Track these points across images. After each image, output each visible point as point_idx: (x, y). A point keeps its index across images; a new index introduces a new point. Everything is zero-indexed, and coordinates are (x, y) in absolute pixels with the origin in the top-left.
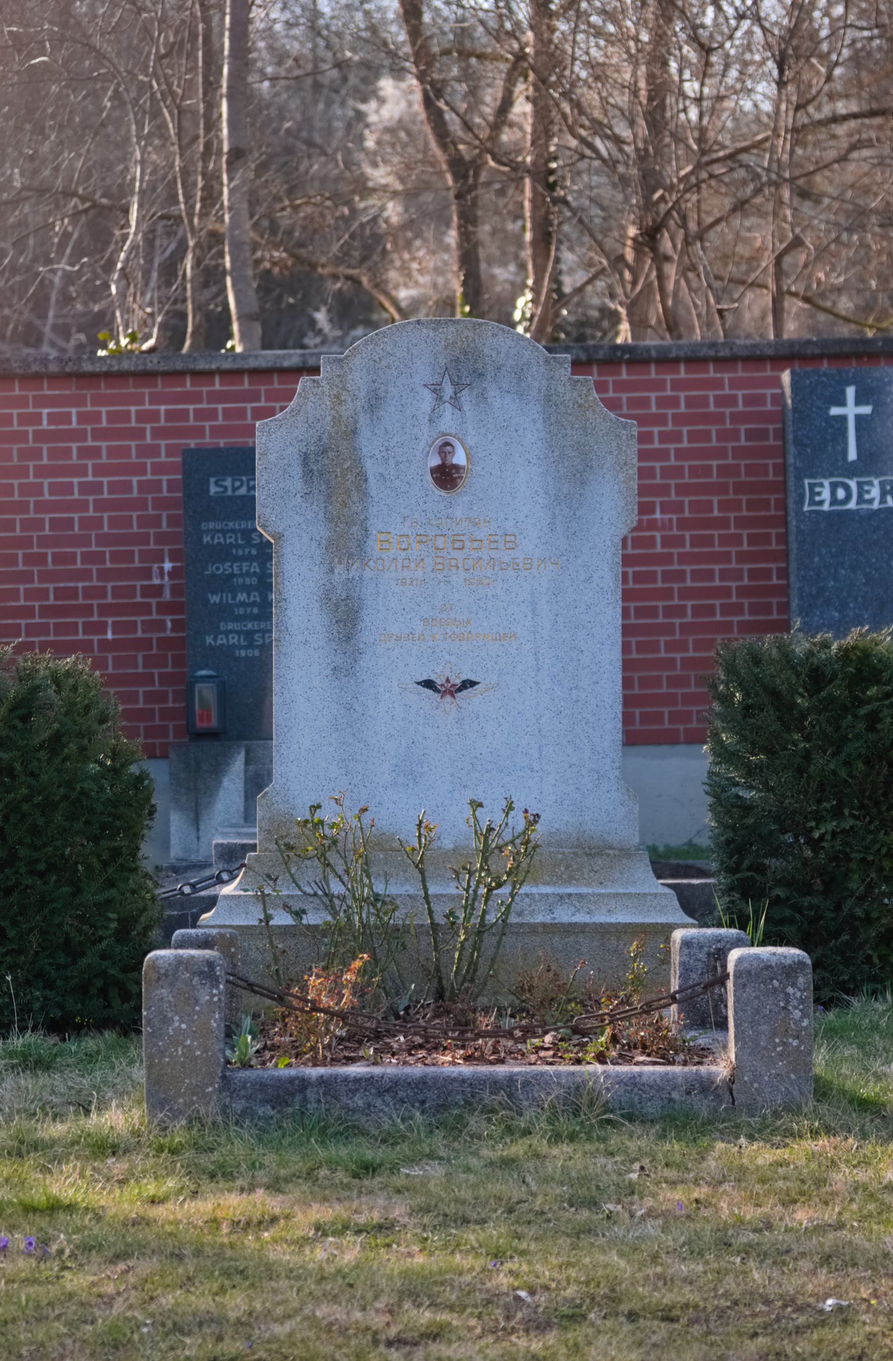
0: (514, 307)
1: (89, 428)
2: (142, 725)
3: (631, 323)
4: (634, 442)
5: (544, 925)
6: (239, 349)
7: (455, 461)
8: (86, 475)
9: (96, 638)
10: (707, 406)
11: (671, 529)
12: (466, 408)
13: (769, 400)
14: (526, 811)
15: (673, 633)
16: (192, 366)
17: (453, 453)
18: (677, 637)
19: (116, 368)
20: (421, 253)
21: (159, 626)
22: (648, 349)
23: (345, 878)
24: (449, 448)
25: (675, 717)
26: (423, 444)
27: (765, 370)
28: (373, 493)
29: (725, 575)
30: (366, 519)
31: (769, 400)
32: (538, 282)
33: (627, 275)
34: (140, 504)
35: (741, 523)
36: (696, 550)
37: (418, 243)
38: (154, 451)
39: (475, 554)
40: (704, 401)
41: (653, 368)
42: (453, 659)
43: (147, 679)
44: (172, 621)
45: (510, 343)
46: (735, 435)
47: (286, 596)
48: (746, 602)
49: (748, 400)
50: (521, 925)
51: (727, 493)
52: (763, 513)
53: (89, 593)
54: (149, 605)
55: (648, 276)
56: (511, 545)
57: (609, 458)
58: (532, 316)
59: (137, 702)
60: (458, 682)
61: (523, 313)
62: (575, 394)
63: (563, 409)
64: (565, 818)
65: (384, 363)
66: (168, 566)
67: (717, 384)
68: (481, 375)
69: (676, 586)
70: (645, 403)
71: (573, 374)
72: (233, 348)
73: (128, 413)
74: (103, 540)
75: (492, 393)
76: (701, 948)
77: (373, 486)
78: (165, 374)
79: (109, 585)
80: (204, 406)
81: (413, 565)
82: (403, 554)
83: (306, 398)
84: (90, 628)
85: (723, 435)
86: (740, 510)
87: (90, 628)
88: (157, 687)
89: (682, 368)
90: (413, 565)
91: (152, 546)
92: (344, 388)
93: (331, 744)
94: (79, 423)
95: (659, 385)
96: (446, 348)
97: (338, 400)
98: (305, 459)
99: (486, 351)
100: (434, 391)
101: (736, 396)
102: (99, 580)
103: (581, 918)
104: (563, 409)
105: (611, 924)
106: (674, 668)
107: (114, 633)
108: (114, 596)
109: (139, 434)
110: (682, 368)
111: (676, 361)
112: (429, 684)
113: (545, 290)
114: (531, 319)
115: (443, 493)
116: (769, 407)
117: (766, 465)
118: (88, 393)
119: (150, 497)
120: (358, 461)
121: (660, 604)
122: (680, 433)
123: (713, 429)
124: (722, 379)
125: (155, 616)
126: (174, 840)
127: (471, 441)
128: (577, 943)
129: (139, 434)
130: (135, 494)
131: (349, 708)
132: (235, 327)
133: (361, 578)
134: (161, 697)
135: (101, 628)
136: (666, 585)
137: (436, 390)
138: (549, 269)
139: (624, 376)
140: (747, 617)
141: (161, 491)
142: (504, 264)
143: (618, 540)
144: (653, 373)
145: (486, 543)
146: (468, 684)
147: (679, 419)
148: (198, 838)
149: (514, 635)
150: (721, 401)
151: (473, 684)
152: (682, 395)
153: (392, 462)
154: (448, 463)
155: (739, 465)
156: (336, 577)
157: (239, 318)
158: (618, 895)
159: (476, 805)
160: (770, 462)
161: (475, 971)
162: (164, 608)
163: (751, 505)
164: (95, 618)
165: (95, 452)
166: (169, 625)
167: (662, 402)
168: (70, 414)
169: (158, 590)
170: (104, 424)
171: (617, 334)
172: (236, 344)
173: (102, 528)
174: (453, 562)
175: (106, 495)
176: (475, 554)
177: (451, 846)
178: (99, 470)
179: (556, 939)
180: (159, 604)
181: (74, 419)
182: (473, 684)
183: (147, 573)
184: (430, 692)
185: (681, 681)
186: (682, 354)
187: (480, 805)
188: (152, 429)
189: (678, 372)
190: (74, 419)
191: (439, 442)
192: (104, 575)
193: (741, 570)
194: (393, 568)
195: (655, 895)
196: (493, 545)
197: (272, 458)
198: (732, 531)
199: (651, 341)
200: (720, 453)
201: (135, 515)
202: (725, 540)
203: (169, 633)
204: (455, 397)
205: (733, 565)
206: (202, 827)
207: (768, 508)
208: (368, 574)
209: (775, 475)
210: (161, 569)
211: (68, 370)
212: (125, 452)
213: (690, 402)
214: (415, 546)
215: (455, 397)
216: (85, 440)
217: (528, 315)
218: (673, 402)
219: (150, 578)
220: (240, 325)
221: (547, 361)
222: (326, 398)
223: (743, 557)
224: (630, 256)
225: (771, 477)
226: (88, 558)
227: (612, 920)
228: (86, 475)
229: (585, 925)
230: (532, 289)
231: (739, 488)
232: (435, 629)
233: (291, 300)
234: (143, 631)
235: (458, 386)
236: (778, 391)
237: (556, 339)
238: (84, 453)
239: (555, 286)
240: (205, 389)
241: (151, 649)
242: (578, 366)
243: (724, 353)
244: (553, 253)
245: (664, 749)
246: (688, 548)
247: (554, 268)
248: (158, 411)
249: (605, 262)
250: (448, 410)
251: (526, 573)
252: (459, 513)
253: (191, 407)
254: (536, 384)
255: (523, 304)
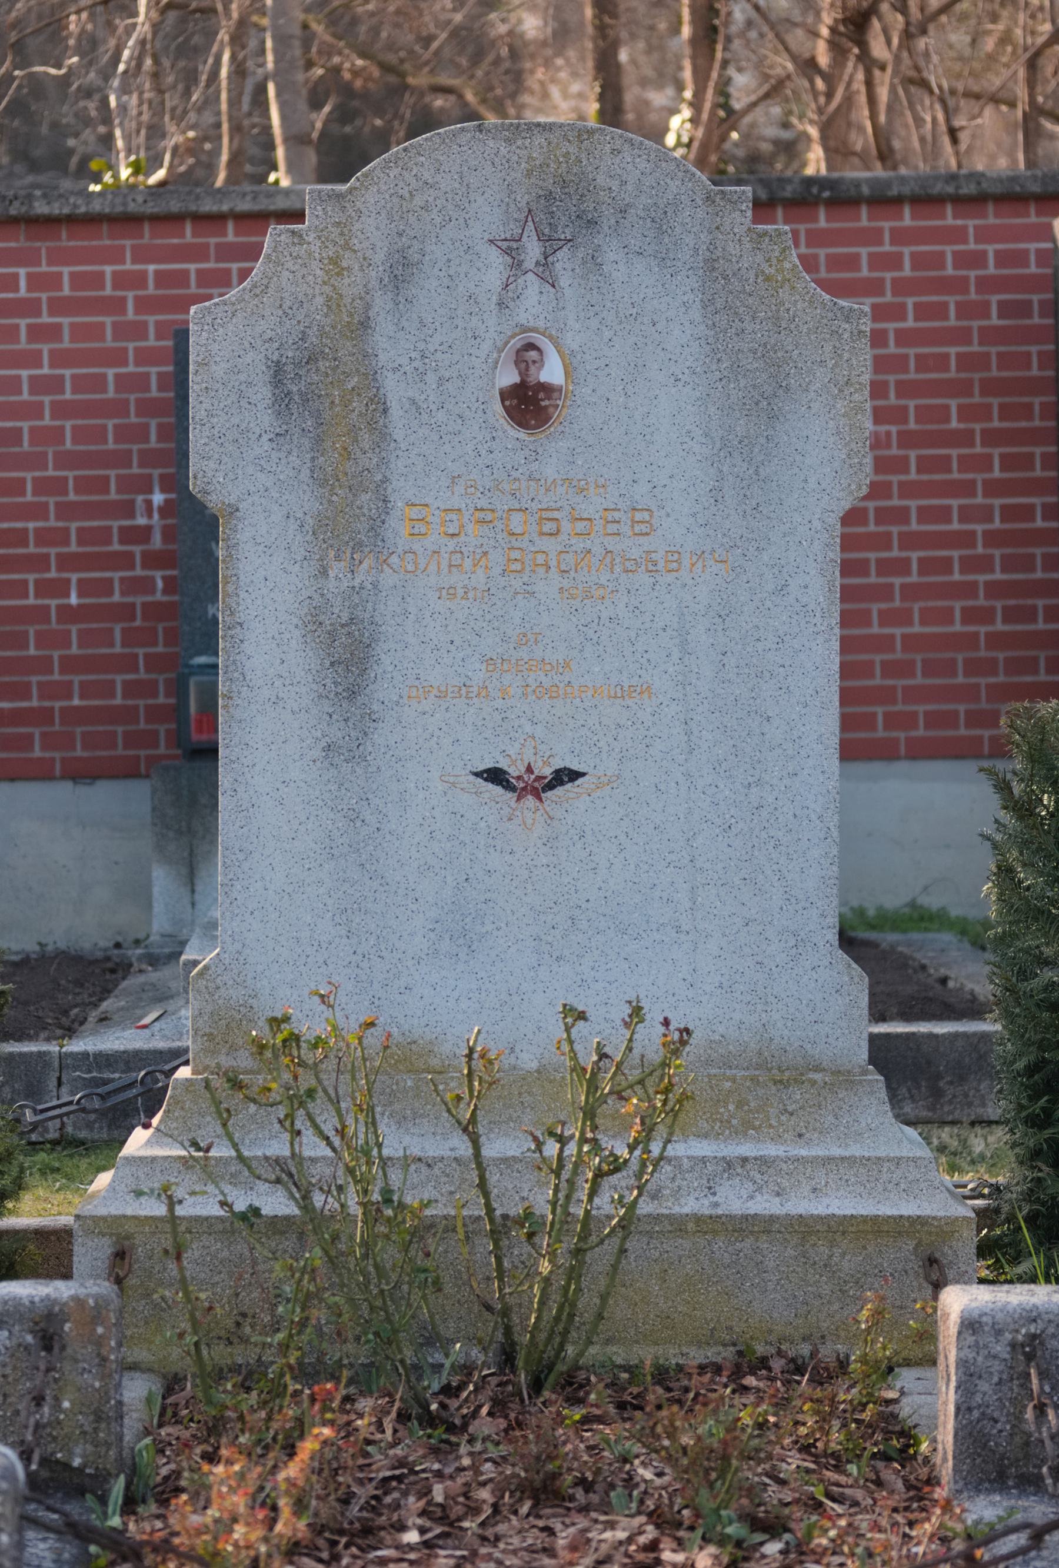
0: (667, 129)
1: (44, 296)
2: (120, 729)
3: (826, 149)
4: (865, 341)
5: (698, 1219)
6: (285, 183)
7: (544, 377)
8: (40, 366)
9: (53, 603)
10: (943, 267)
11: (888, 446)
12: (564, 281)
13: (1033, 258)
14: (666, 1022)
15: (890, 598)
16: (193, 208)
17: (540, 363)
18: (897, 603)
19: (83, 209)
20: (563, 75)
21: (144, 585)
22: (857, 184)
23: (337, 1141)
24: (533, 354)
25: (891, 721)
26: (487, 346)
27: (1028, 216)
28: (398, 434)
29: (966, 514)
30: (385, 480)
31: (1033, 258)
32: (699, 94)
33: (820, 84)
34: (118, 408)
35: (991, 438)
36: (925, 477)
37: (559, 62)
38: (138, 330)
39: (579, 544)
40: (938, 260)
41: (864, 210)
42: (539, 731)
43: (129, 663)
44: (164, 578)
45: (642, 165)
46: (983, 310)
47: (241, 617)
48: (997, 553)
49: (1003, 259)
50: (657, 1218)
51: (971, 395)
52: (1024, 424)
53: (44, 537)
54: (131, 555)
55: (849, 84)
56: (643, 528)
57: (819, 372)
58: (691, 140)
59: (113, 696)
60: (548, 772)
61: (679, 136)
62: (759, 258)
63: (736, 284)
64: (737, 1016)
65: (418, 201)
66: (158, 498)
67: (958, 235)
68: (592, 223)
69: (895, 530)
70: (852, 263)
71: (756, 220)
72: (277, 182)
73: (101, 275)
74: (65, 460)
75: (611, 256)
76: (998, 1333)
77: (398, 418)
78: (155, 219)
79: (74, 526)
80: (211, 265)
81: (468, 563)
82: (452, 543)
83: (278, 263)
84: (45, 588)
85: (965, 310)
86: (990, 419)
87: (45, 588)
88: (142, 675)
89: (907, 211)
90: (468, 563)
91: (135, 470)
92: (347, 247)
93: (320, 882)
94: (29, 289)
95: (873, 237)
96: (529, 174)
97: (336, 266)
98: (277, 373)
99: (601, 180)
100: (508, 252)
101: (984, 253)
102: (58, 518)
103: (765, 1205)
104: (736, 284)
105: (820, 1218)
106: (892, 649)
107: (80, 595)
108: (80, 542)
109: (117, 306)
110: (907, 211)
111: (898, 201)
112: (495, 776)
113: (707, 106)
114: (688, 145)
115: (522, 434)
116: (1033, 269)
117: (1029, 354)
118: (43, 247)
119: (132, 397)
120: (371, 377)
121: (872, 556)
122: (903, 306)
123: (952, 300)
124: (965, 228)
125: (138, 572)
126: (158, 907)
127: (572, 341)
128: (757, 1250)
129: (118, 304)
130: (111, 393)
131: (354, 818)
132: (280, 153)
133: (375, 585)
134: (148, 689)
135: (61, 588)
136: (881, 529)
137: (511, 249)
138: (714, 75)
139: (822, 223)
140: (998, 576)
141: (148, 389)
142: (660, 87)
143: (834, 519)
144: (864, 219)
145: (599, 524)
146: (566, 776)
147: (901, 287)
148: (193, 904)
149: (647, 690)
150: (964, 260)
151: (574, 775)
152: (907, 251)
153: (431, 378)
154: (532, 380)
155: (988, 355)
156: (332, 584)
157: (286, 140)
158: (830, 1159)
159: (575, 1015)
160: (1034, 349)
161: (571, 1316)
162: (152, 560)
163: (1006, 412)
164: (53, 574)
165: (53, 332)
166: (160, 584)
167: (878, 262)
168: (16, 276)
169: (145, 534)
170: (66, 291)
171: (804, 165)
172: (281, 177)
173: (63, 442)
174: (540, 559)
175: (68, 395)
176: (579, 544)
177: (534, 1065)
178: (59, 359)
179: (720, 1243)
180: (145, 555)
181: (23, 283)
182: (574, 775)
183: (127, 509)
184: (498, 790)
185: (903, 669)
186: (906, 190)
187: (582, 1016)
188: (137, 298)
189: (901, 218)
190: (23, 283)
191: (516, 343)
192: (66, 511)
193: (991, 507)
194: (433, 567)
195: (898, 1161)
196: (612, 528)
197: (219, 370)
198: (978, 449)
199: (854, 173)
200: (962, 336)
201: (110, 424)
202: (966, 463)
203: (159, 597)
204: (545, 263)
205: (979, 500)
206: (199, 888)
207: (1030, 417)
208: (388, 578)
209: (1041, 368)
210: (149, 503)
211: (13, 212)
212: (95, 332)
213: (918, 261)
214: (470, 528)
215: (545, 263)
216: (39, 314)
217: (685, 139)
218: (894, 262)
219: (132, 515)
220: (287, 150)
221: (709, 199)
222: (315, 265)
223: (993, 488)
224: (823, 59)
225: (1035, 372)
226: (43, 486)
227: (819, 1207)
228: (40, 366)
229: (772, 1219)
230: (691, 104)
231: (989, 387)
232: (507, 678)
233: (378, 122)
234: (123, 593)
235: (551, 243)
236: (1048, 245)
237: (723, 172)
238: (36, 333)
239: (722, 100)
240: (213, 241)
241: (133, 618)
242: (763, 208)
243: (969, 189)
244: (719, 55)
245: (877, 767)
246: (913, 475)
247: (720, 76)
248: (145, 273)
249: (790, 66)
250: (531, 285)
251: (670, 578)
252: (550, 471)
253: (192, 267)
254: (689, 240)
255: (679, 126)
